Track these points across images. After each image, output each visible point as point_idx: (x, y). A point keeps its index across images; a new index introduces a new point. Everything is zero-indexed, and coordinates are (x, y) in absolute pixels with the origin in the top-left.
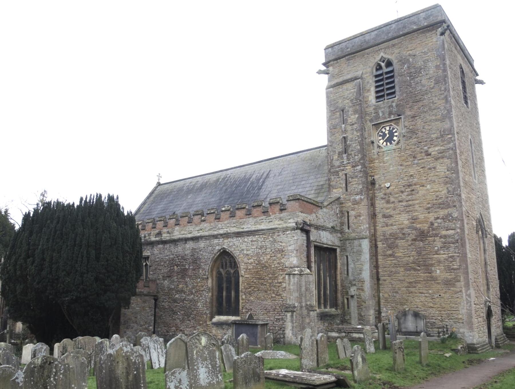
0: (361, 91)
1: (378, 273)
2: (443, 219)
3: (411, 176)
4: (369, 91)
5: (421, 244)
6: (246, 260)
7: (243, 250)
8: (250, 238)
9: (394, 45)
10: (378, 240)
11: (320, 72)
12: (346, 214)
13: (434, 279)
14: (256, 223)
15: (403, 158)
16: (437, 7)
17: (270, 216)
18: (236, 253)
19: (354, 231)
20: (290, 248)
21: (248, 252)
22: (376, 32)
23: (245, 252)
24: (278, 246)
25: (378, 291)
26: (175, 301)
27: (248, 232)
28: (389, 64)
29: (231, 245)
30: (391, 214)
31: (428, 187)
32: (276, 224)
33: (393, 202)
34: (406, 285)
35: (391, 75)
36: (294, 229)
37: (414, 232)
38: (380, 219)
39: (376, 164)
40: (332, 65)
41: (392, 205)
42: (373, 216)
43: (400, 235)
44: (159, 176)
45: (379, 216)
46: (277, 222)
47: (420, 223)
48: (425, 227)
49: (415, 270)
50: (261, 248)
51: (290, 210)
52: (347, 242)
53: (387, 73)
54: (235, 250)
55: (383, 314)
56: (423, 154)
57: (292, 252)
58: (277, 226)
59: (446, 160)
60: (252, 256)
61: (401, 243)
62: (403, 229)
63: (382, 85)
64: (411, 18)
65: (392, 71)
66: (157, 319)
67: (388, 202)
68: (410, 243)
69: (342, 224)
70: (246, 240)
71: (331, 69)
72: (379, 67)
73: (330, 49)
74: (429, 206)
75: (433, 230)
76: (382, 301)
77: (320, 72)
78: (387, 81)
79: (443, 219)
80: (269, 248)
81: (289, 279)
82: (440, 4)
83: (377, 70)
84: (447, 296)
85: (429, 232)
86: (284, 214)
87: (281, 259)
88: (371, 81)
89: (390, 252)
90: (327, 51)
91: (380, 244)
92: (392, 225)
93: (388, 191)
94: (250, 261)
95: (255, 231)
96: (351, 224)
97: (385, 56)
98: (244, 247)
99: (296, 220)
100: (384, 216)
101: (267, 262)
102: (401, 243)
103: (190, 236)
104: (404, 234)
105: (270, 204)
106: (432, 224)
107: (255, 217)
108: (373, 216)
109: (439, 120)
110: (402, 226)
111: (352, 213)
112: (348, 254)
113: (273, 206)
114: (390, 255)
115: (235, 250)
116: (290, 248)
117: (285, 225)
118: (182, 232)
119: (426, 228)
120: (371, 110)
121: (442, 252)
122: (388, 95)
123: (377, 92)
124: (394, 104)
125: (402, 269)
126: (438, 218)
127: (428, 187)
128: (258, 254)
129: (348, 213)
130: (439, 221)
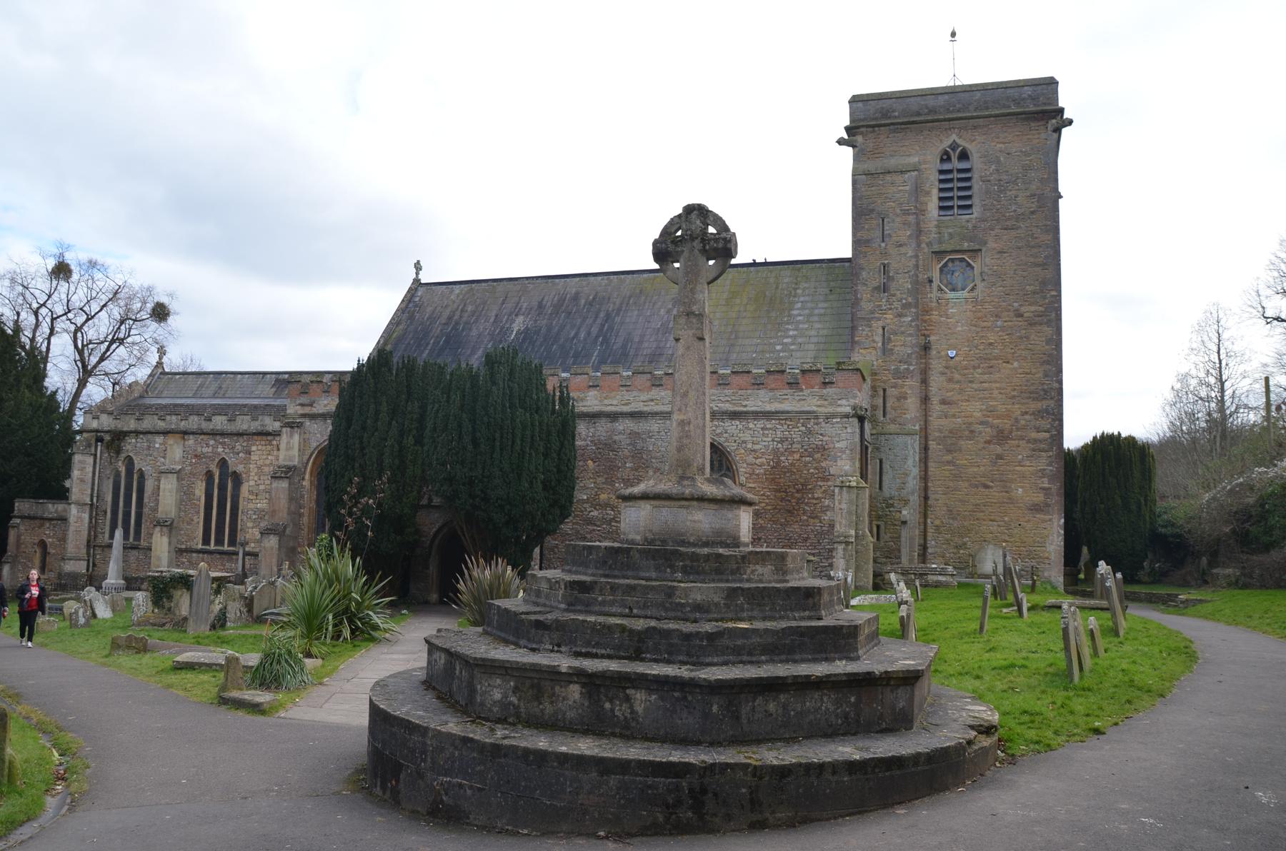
0: (918, 190)
1: (926, 489)
2: (1033, 414)
3: (991, 344)
4: (928, 193)
5: (999, 449)
6: (750, 459)
7: (744, 442)
8: (760, 424)
9: (975, 127)
10: (931, 438)
11: (841, 142)
12: (881, 393)
13: (1011, 501)
14: (775, 399)
15: (980, 314)
16: (1051, 83)
17: (802, 390)
18: (731, 446)
19: (893, 421)
20: (837, 445)
21: (756, 447)
22: (946, 97)
23: (750, 446)
24: (816, 441)
25: (925, 516)
26: (590, 521)
27: (753, 412)
28: (964, 156)
29: (718, 431)
30: (954, 398)
31: (1016, 364)
32: (811, 404)
33: (958, 382)
34: (971, 507)
35: (966, 177)
36: (847, 416)
37: (988, 430)
38: (936, 407)
39: (935, 316)
40: (862, 133)
41: (957, 386)
42: (925, 400)
43: (967, 433)
44: (418, 267)
45: (935, 400)
46: (815, 401)
47: (998, 418)
48: (1006, 424)
49: (986, 487)
50: (782, 442)
51: (841, 385)
52: (883, 438)
53: (959, 171)
54: (727, 440)
55: (930, 551)
56: (1011, 314)
57: (843, 452)
58: (815, 409)
59: (1045, 328)
60: (763, 454)
61: (965, 444)
62: (970, 424)
63: (951, 189)
64: (1009, 91)
65: (968, 170)
66: (546, 552)
67: (950, 380)
68: (981, 446)
69: (874, 408)
70: (751, 425)
71: (859, 139)
72: (945, 157)
73: (860, 105)
74: (1015, 393)
75: (1018, 429)
76: (930, 531)
77: (841, 142)
78: (960, 185)
79: (1033, 414)
80: (799, 442)
81: (840, 493)
82: (1057, 78)
83: (942, 160)
84: (1029, 526)
85: (1011, 432)
86: (829, 391)
87: (820, 462)
88: (932, 178)
89: (949, 458)
90: (855, 105)
91: (932, 445)
92: (954, 416)
93: (952, 363)
94: (758, 461)
95: (769, 412)
96: (888, 409)
97: (959, 141)
98: (747, 436)
99: (852, 402)
100: (943, 402)
101: (792, 464)
102: (965, 444)
103: (626, 409)
104: (972, 432)
105: (803, 372)
106: (1017, 420)
107: (772, 390)
108: (925, 400)
109: (1039, 265)
110: (970, 420)
111: (890, 391)
112: (883, 456)
113: (808, 376)
114: (948, 462)
115: (727, 440)
116: (837, 445)
117: (830, 409)
118: (606, 402)
119: (1007, 426)
120: (932, 225)
121: (1028, 463)
122: (959, 207)
123: (941, 199)
124: (970, 225)
125: (966, 484)
126: (1026, 413)
127: (1016, 364)
128: (776, 452)
129: (884, 390)
130: (1027, 417)
